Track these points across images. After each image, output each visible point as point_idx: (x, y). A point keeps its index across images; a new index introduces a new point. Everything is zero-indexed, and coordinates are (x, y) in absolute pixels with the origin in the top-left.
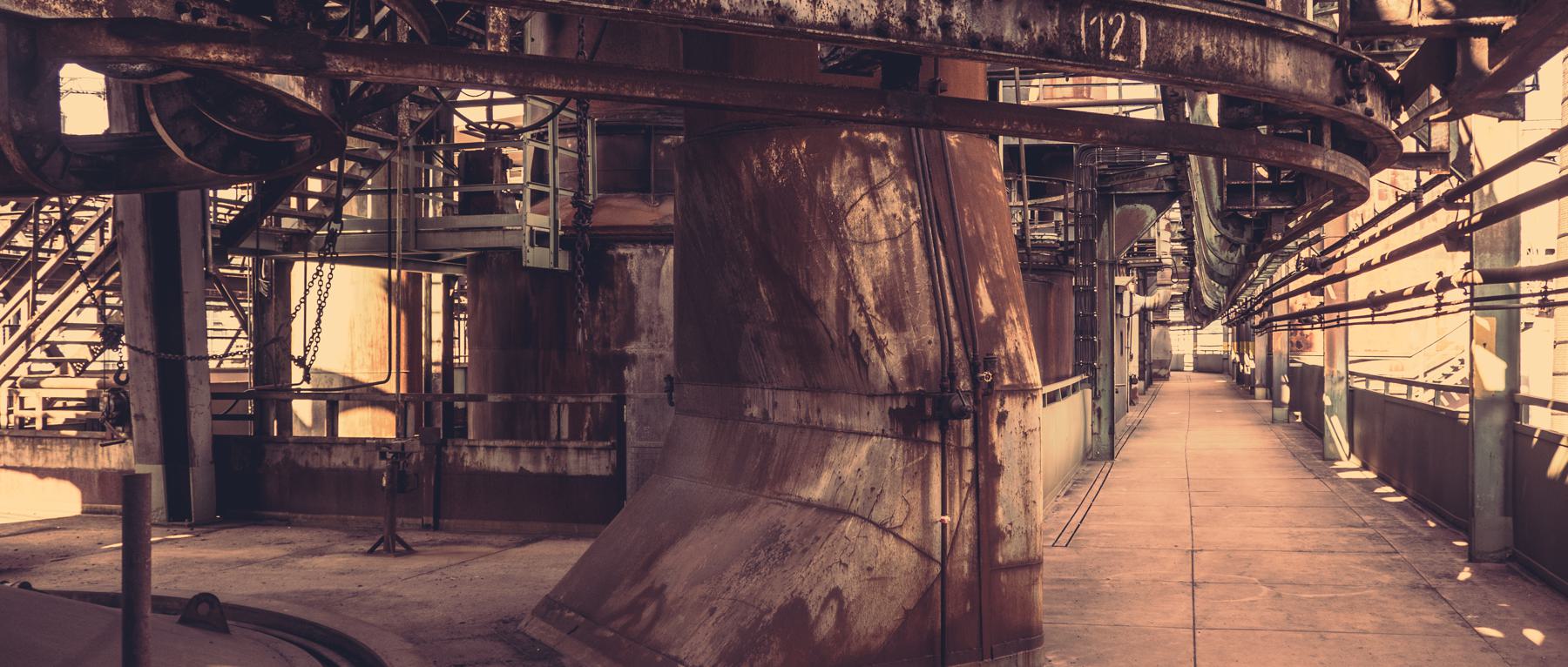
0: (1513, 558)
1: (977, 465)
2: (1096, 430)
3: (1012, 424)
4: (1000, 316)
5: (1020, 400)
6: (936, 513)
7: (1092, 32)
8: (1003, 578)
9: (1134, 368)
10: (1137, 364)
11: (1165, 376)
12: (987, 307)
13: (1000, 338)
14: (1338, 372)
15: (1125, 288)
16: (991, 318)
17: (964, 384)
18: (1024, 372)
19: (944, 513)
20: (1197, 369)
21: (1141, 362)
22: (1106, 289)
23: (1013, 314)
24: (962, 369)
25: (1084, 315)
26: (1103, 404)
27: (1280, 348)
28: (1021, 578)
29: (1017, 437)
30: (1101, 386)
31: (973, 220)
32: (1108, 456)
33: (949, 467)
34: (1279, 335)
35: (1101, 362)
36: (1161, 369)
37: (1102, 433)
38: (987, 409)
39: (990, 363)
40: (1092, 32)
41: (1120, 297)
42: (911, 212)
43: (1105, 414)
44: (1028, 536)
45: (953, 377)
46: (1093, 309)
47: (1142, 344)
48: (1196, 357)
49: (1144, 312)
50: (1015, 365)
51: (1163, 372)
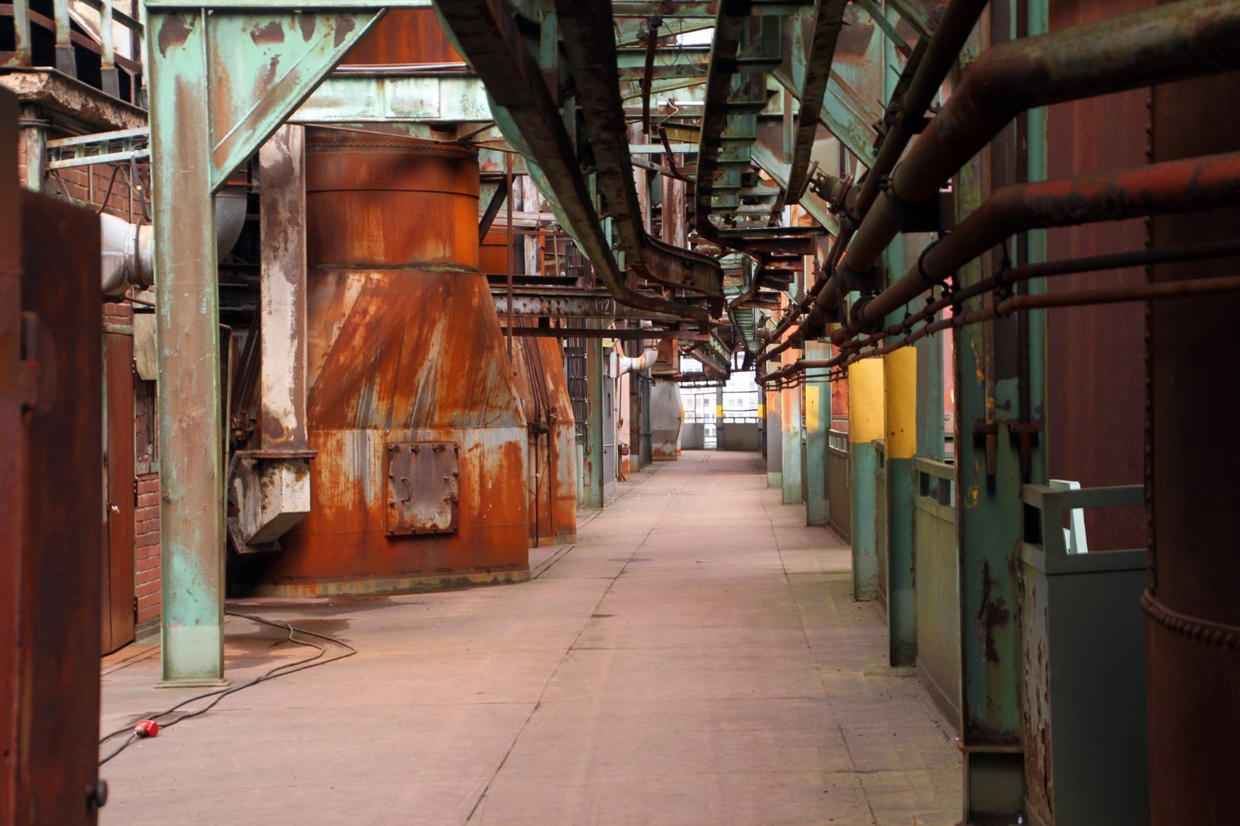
0: (828, 524)
1: (549, 454)
2: (587, 482)
3: (563, 437)
4: (557, 389)
5: (566, 426)
6: (533, 473)
7: (599, 307)
8: (560, 503)
9: (624, 437)
10: (628, 431)
11: (670, 454)
12: (551, 386)
13: (558, 400)
14: (794, 428)
15: (611, 350)
16: (553, 391)
17: (543, 419)
18: (567, 414)
19: (537, 472)
20: (723, 445)
21: (634, 432)
22: (595, 355)
23: (562, 389)
24: (543, 412)
25: (577, 379)
26: (592, 458)
27: (774, 409)
28: (568, 503)
29: (565, 443)
30: (590, 443)
31: (543, 346)
32: (599, 505)
33: (539, 453)
34: (773, 395)
35: (591, 421)
36: (666, 442)
37: (593, 484)
38: (553, 430)
39: (554, 410)
40: (599, 307)
41: (607, 357)
42: (518, 345)
43: (595, 468)
44: (570, 485)
45: (540, 416)
46: (584, 373)
47: (635, 407)
48: (722, 428)
49: (635, 374)
50: (563, 411)
51: (668, 448)
